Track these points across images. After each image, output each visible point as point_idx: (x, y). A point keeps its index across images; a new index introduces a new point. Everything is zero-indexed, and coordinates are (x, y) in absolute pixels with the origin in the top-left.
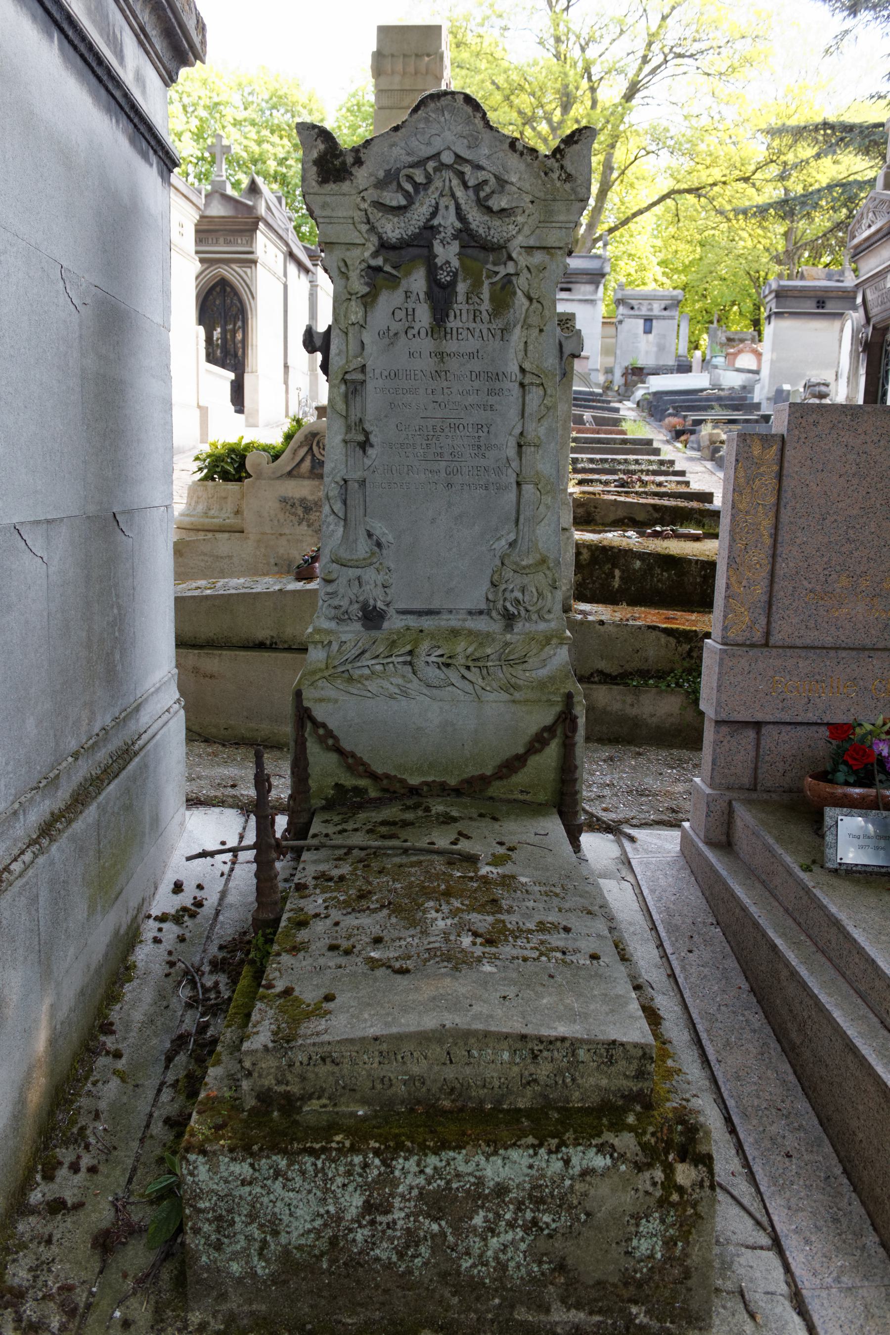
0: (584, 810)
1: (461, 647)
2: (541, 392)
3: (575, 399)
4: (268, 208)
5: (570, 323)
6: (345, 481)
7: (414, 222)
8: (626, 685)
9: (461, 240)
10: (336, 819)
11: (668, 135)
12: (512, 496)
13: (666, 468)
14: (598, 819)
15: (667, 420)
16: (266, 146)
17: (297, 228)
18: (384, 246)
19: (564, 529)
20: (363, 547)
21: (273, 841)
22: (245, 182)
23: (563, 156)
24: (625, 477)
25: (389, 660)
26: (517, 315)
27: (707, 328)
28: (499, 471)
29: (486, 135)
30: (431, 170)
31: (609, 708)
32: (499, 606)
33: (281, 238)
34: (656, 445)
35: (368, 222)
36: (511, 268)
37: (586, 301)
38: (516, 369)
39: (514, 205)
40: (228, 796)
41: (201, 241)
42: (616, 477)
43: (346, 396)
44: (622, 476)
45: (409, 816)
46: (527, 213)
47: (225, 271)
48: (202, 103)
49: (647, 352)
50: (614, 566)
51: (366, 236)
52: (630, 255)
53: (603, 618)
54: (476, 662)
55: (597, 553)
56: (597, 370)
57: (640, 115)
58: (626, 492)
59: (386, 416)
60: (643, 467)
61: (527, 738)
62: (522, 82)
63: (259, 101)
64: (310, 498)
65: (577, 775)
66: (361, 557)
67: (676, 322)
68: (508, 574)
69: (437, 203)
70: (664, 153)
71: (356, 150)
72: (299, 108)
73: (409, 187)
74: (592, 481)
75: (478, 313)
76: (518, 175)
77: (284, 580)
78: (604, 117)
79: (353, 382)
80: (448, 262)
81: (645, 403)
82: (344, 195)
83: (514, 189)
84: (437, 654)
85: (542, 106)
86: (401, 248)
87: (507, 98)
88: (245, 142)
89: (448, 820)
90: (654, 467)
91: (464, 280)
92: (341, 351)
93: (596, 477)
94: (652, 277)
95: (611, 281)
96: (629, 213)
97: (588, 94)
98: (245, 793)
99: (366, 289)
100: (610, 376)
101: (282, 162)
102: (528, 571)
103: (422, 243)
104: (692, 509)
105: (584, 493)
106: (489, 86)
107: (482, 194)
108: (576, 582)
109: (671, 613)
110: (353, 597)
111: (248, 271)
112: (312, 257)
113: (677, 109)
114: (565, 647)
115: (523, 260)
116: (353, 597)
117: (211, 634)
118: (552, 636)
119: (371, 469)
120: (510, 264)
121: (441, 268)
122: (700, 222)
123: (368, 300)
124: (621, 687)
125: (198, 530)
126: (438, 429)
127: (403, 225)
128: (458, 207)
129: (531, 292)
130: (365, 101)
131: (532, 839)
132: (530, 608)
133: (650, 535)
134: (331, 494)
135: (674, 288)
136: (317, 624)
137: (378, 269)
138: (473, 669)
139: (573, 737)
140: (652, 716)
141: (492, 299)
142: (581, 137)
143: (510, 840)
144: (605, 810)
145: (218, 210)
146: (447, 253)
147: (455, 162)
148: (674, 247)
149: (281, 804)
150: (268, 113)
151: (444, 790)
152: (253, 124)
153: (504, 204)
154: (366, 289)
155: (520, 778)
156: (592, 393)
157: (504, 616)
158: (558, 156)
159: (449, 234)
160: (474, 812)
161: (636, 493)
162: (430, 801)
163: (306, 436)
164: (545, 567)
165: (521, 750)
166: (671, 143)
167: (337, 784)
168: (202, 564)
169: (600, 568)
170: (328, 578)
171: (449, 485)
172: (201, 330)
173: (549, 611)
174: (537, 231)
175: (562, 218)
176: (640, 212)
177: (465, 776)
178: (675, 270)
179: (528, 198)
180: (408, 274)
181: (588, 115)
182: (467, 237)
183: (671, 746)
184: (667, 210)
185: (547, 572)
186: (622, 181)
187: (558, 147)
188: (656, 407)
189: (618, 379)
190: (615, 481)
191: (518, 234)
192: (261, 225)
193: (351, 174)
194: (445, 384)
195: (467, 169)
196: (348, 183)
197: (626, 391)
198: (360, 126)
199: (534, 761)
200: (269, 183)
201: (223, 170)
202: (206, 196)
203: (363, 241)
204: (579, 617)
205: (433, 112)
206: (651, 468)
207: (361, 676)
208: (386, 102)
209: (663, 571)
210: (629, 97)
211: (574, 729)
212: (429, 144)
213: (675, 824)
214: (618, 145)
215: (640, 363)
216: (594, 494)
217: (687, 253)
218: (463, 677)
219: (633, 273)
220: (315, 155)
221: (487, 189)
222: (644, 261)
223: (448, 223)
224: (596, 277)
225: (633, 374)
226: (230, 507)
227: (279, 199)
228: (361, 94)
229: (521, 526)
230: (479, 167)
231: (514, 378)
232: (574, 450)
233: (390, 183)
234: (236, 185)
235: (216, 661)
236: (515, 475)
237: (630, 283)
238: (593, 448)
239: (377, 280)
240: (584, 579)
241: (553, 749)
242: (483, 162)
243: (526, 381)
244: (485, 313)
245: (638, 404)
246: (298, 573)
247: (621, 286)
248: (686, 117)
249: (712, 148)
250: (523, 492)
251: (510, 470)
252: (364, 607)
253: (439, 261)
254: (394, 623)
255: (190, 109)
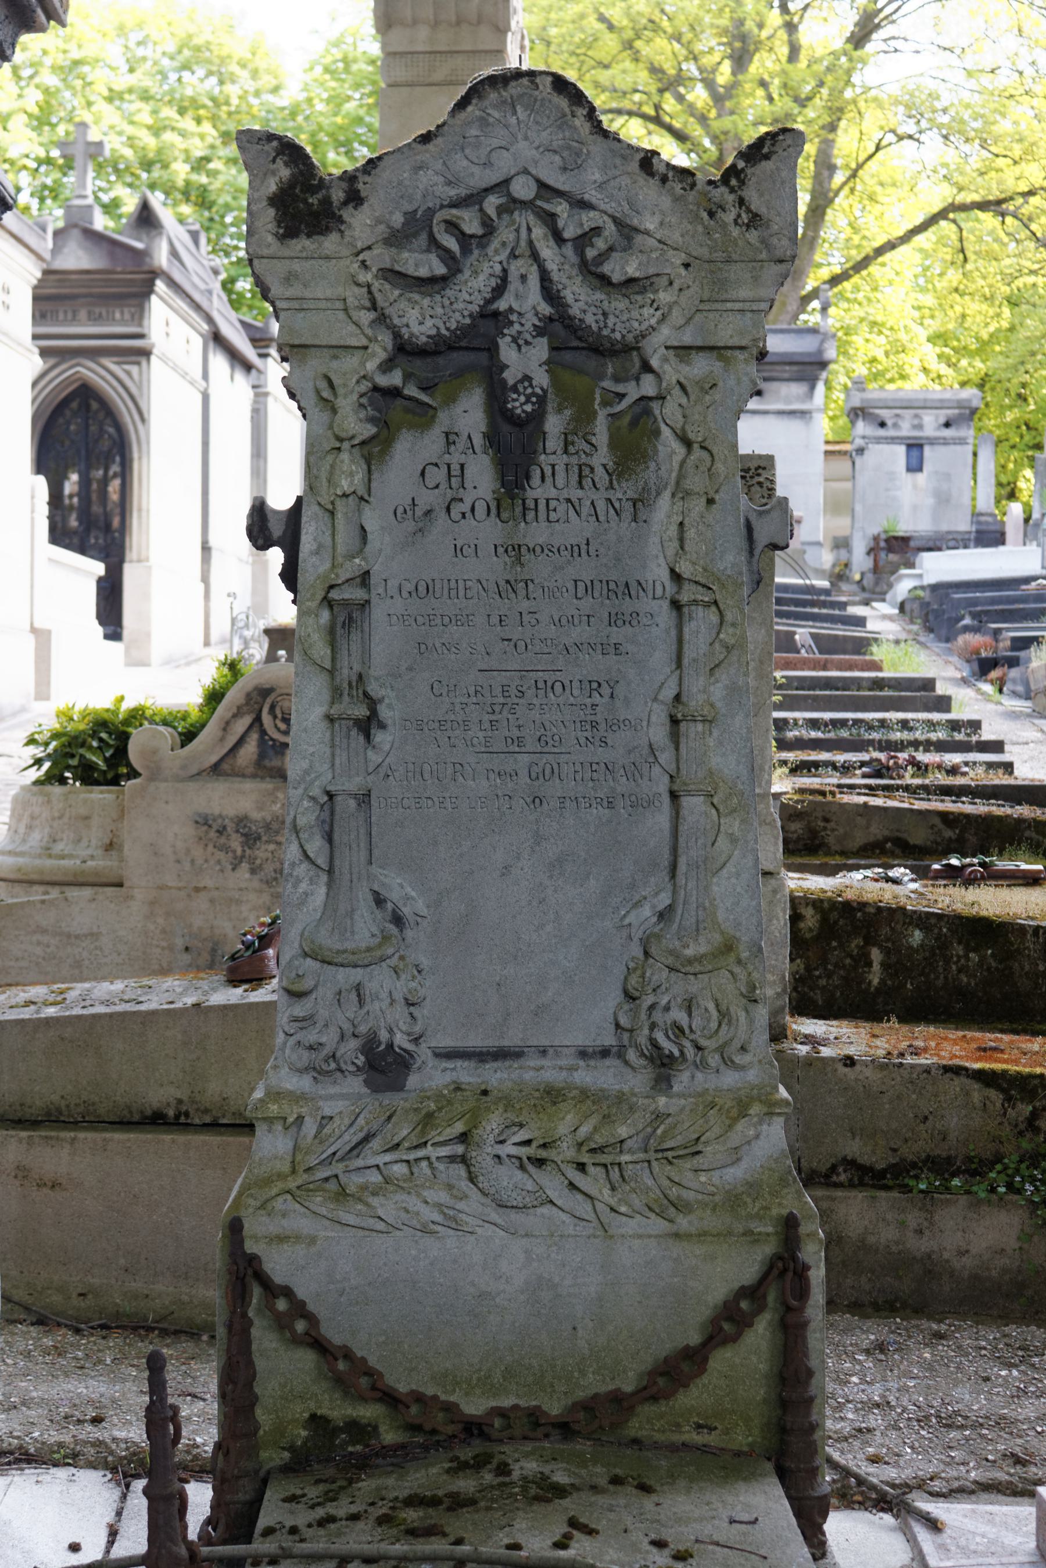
0: (829, 1460)
1: (567, 1125)
2: (714, 618)
3: (779, 601)
4: (174, 253)
5: (765, 474)
6: (331, 796)
7: (460, 306)
8: (906, 1189)
9: (552, 337)
10: (313, 1492)
11: (938, 105)
12: (662, 819)
13: (966, 736)
14: (861, 1481)
15: (961, 640)
16: (168, 137)
17: (228, 285)
18: (404, 350)
19: (766, 874)
20: (366, 926)
21: (183, 1552)
22: (130, 205)
23: (742, 183)
24: (882, 756)
25: (420, 1153)
26: (663, 473)
27: (1032, 459)
28: (634, 771)
29: (597, 147)
30: (491, 212)
31: (871, 1240)
32: (642, 1039)
33: (197, 307)
34: (941, 689)
35: (374, 307)
36: (648, 386)
37: (792, 413)
38: (665, 575)
39: (652, 271)
40: (86, 1443)
41: (43, 316)
42: (865, 757)
43: (332, 631)
44: (876, 755)
45: (466, 1485)
46: (676, 286)
47: (89, 371)
48: (48, 61)
49: (915, 508)
50: (870, 941)
51: (369, 332)
52: (874, 323)
53: (851, 1051)
54: (596, 1154)
55: (834, 915)
56: (818, 544)
57: (881, 71)
58: (886, 788)
59: (410, 669)
60: (918, 735)
61: (705, 1313)
62: (657, 16)
63: (158, 55)
64: (255, 815)
65: (813, 1390)
66: (364, 945)
67: (970, 449)
68: (658, 974)
69: (505, 271)
70: (932, 139)
71: (349, 178)
72: (234, 68)
73: (451, 243)
74: (816, 765)
75: (586, 471)
76: (657, 219)
77: (205, 985)
78: (814, 75)
79: (345, 603)
80: (527, 378)
81: (916, 606)
82: (328, 258)
83: (652, 242)
84: (517, 1139)
85: (695, 59)
86: (436, 353)
87: (628, 45)
88: (130, 130)
89: (548, 1492)
90: (941, 735)
91: (559, 410)
92: (320, 546)
93: (824, 756)
94: (918, 365)
95: (839, 374)
96: (868, 249)
97: (783, 35)
98: (121, 1434)
99: (370, 430)
100: (843, 554)
101: (200, 164)
102: (697, 968)
103: (476, 343)
104: (1020, 821)
105: (801, 791)
106: (592, 23)
107: (590, 253)
108: (793, 974)
109: (990, 1038)
110: (347, 1026)
111: (134, 369)
112: (259, 340)
113: (952, 59)
114: (778, 1123)
115: (671, 372)
116: (347, 1026)
117: (55, 1098)
118: (751, 1099)
119: (382, 771)
120: (648, 379)
121: (514, 389)
122: (1007, 261)
123: (374, 451)
124: (895, 1194)
125: (31, 883)
126: (513, 691)
127: (439, 311)
128: (545, 277)
129: (689, 429)
130: (358, 53)
131: (723, 1532)
132: (703, 1042)
133: (938, 875)
134: (302, 821)
135: (963, 384)
136: (273, 1082)
137: (394, 393)
138: (591, 1169)
139: (801, 1309)
140: (962, 1253)
141: (614, 444)
142: (775, 145)
143: (680, 1536)
144: (874, 1460)
145: (77, 258)
146: (525, 361)
147: (538, 196)
148: (958, 309)
149: (196, 1457)
150: (173, 77)
151: (537, 1424)
152: (146, 96)
153: (632, 270)
154: (370, 430)
155: (694, 1398)
156: (810, 589)
157: (651, 1059)
158: (734, 182)
159: (528, 326)
160: (600, 1474)
161: (907, 788)
162: (508, 1451)
163: (248, 696)
164: (732, 958)
165: (695, 1339)
166: (945, 119)
167: (313, 1417)
168: (39, 951)
169: (841, 945)
170: (296, 988)
171: (537, 800)
172: (41, 483)
173: (743, 1049)
174: (698, 317)
175: (743, 293)
176: (891, 246)
177: (581, 1395)
178: (962, 351)
179: (678, 258)
180: (451, 400)
181: (784, 72)
182: (562, 330)
183: (1005, 1318)
184: (942, 241)
185: (737, 970)
186: (852, 190)
187: (733, 166)
188: (938, 614)
189: (860, 561)
190: (863, 764)
191: (661, 325)
192: (160, 285)
193: (340, 220)
194: (525, 605)
195: (561, 208)
196: (334, 236)
197: (877, 583)
198: (349, 98)
199: (721, 1360)
200: (175, 205)
201: (89, 185)
202: (57, 233)
203: (364, 342)
204: (803, 1050)
205: (495, 107)
206: (933, 736)
207: (364, 1188)
208: (401, 74)
209: (968, 949)
210: (860, 38)
211: (802, 1291)
212: (487, 164)
213: (1023, 1491)
214: (843, 124)
215: (903, 527)
216: (823, 793)
217: (984, 319)
218: (572, 1186)
219: (881, 357)
220: (272, 187)
221: (600, 244)
222: (902, 336)
223: (526, 307)
224: (810, 369)
225: (890, 549)
226: (96, 836)
227: (195, 236)
228: (350, 40)
229: (681, 880)
230: (584, 205)
231: (659, 592)
232: (779, 707)
233: (415, 235)
234: (111, 208)
235: (66, 1150)
236: (666, 779)
237: (876, 376)
238: (815, 698)
239: (392, 412)
240: (808, 969)
241: (761, 1334)
242: (591, 195)
243: (684, 598)
244: (600, 471)
245: (902, 607)
246: (231, 970)
247: (859, 384)
248: (970, 74)
249: (1023, 127)
250: (684, 812)
251: (656, 770)
252: (370, 1046)
253: (510, 376)
254: (430, 1077)
255: (26, 73)
